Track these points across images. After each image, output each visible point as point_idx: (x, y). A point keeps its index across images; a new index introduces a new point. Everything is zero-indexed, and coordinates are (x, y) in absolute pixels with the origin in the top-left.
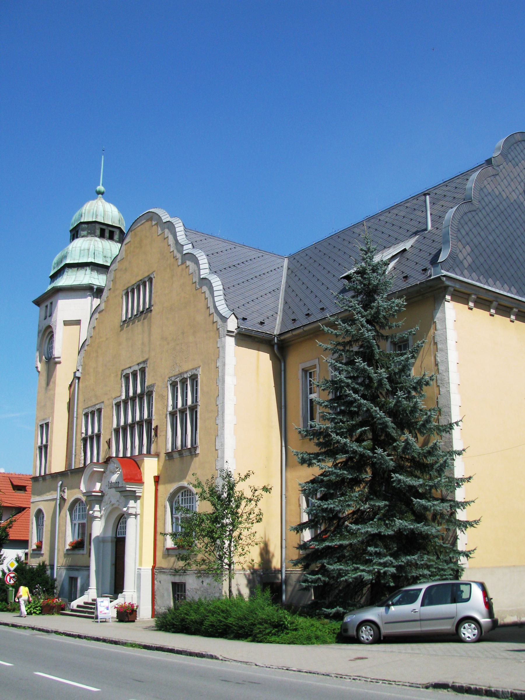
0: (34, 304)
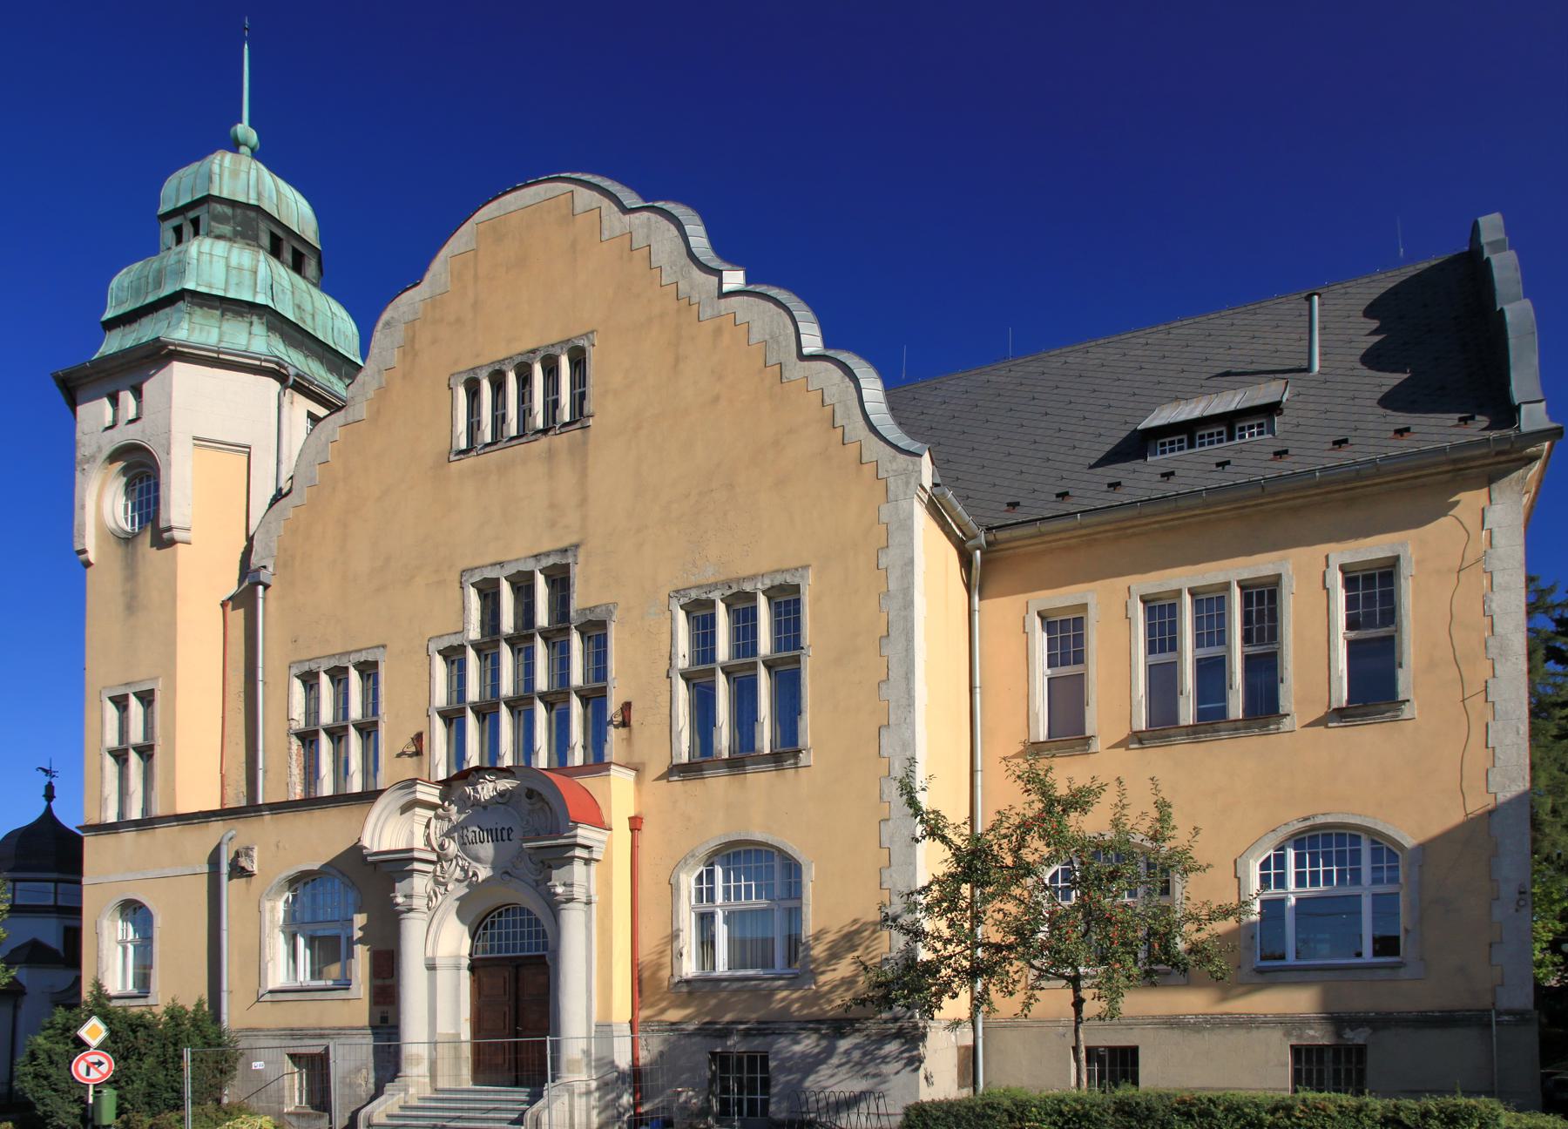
0: (53, 383)
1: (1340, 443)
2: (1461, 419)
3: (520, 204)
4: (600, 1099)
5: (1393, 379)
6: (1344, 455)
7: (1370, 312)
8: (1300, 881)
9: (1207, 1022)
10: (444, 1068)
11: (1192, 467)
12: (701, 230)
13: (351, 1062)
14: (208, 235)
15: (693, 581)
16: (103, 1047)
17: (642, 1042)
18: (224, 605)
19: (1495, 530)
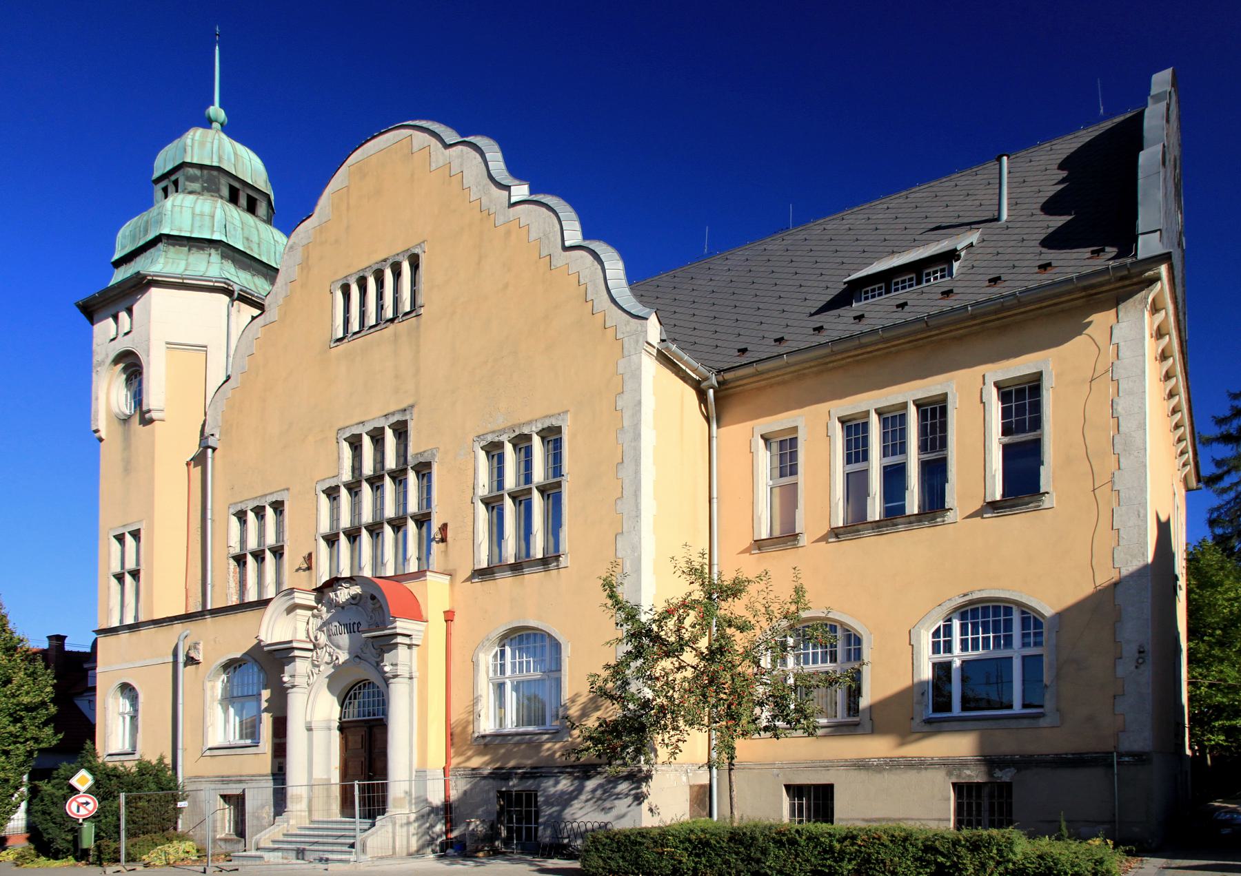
0: (78, 310)
1: (995, 281)
2: (1093, 252)
3: (377, 149)
4: (420, 826)
5: (1059, 221)
6: (996, 290)
7: (1061, 167)
8: (964, 647)
9: (886, 764)
10: (318, 804)
11: (878, 310)
12: (499, 156)
13: (259, 798)
14: (183, 192)
15: (490, 427)
16: (89, 791)
17: (452, 784)
18: (188, 464)
19: (1121, 344)
